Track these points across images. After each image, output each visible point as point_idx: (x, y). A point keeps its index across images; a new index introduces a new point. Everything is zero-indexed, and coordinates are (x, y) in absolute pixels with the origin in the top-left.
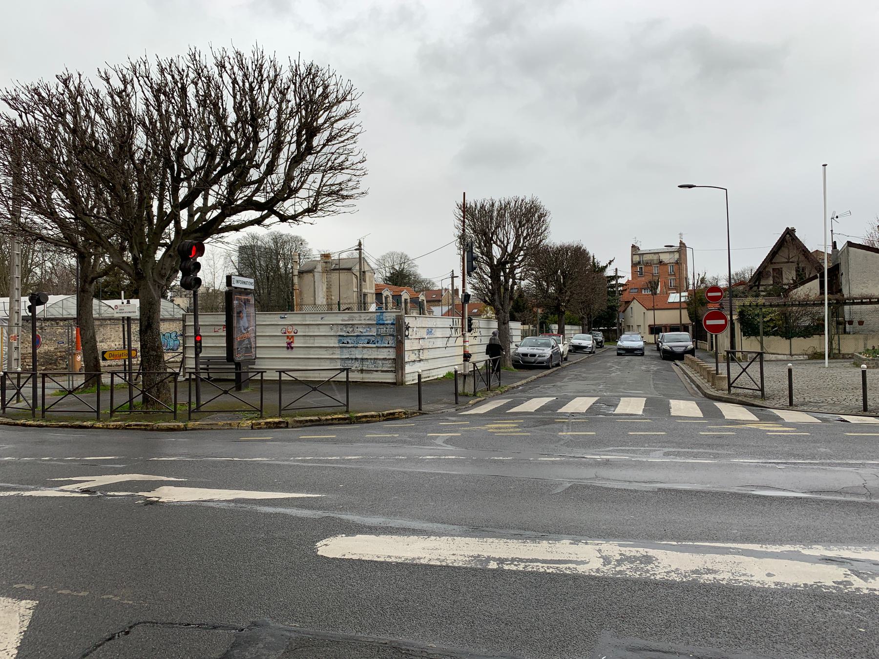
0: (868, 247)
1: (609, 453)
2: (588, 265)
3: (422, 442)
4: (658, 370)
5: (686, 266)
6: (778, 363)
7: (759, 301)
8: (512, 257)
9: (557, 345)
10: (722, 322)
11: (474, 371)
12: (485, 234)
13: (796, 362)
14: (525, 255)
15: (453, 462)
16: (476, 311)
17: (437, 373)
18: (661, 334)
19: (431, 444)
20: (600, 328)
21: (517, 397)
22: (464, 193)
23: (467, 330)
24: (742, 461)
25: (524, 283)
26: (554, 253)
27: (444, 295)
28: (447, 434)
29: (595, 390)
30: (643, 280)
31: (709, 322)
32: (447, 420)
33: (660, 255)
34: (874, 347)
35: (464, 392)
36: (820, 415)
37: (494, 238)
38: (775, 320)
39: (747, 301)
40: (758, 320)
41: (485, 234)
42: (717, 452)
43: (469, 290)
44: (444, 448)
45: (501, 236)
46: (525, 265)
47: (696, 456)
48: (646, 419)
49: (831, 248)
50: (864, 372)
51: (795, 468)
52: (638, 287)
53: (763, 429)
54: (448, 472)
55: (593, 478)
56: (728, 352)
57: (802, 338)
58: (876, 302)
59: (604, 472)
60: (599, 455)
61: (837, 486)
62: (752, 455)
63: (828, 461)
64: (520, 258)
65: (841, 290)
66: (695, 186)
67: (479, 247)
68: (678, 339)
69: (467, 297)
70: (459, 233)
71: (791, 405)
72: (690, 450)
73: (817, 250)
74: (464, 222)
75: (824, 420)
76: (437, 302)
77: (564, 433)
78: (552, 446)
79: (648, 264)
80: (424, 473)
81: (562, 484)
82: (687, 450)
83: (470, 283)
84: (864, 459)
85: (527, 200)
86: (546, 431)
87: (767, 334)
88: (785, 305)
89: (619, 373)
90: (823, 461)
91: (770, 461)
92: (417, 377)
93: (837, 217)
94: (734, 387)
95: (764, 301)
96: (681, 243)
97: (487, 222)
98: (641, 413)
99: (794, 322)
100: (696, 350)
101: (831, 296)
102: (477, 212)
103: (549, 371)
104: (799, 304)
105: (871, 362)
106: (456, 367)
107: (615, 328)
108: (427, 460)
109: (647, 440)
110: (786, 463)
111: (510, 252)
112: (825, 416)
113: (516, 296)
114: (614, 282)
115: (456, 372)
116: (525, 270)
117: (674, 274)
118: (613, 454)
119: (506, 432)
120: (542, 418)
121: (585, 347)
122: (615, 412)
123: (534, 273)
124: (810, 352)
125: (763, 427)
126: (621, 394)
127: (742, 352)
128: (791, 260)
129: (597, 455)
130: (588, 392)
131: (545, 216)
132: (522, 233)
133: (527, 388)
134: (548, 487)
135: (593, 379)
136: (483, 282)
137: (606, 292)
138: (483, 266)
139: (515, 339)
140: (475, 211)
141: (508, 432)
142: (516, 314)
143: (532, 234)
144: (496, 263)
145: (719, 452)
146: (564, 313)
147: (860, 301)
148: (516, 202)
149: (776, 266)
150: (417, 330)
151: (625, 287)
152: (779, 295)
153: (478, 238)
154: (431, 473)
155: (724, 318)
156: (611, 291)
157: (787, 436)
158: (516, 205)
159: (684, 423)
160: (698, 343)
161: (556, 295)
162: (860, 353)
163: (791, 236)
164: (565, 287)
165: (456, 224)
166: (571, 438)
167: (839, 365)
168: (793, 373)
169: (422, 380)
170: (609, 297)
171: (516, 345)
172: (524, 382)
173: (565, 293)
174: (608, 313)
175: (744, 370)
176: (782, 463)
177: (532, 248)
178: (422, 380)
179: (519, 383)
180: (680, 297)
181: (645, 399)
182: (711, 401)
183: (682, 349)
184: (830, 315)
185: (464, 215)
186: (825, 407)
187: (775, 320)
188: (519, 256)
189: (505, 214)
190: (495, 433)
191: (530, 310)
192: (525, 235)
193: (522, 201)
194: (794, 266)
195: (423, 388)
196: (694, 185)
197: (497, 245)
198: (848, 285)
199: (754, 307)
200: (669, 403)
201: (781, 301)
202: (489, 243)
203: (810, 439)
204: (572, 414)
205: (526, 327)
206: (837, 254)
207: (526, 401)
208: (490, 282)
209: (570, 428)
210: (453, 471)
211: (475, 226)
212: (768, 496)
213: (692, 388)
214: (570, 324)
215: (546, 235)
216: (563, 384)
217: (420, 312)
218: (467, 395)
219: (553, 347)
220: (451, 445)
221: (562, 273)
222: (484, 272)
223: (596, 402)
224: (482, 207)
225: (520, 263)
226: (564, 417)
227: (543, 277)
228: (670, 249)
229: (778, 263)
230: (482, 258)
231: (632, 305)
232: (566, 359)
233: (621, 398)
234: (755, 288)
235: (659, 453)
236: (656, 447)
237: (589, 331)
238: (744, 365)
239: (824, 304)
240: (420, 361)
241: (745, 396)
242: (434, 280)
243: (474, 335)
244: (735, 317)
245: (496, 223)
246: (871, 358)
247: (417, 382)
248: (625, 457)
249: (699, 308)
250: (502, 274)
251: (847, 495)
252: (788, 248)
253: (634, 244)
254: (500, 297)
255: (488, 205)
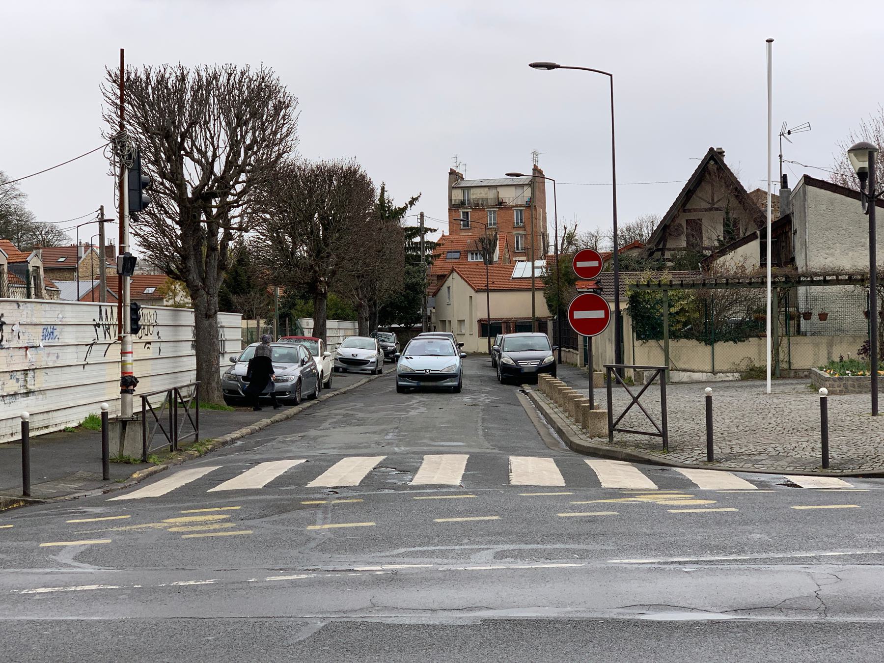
0: (836, 185)
1: (398, 560)
2: (370, 205)
3: (27, 560)
4: (491, 402)
5: (545, 213)
6: (695, 386)
7: (662, 277)
8: (224, 184)
9: (310, 358)
10: (600, 314)
11: (144, 411)
12: (167, 136)
13: (721, 385)
14: (249, 182)
15: (94, 596)
16: (151, 290)
17: (64, 419)
18: (499, 336)
19: (47, 564)
20: (393, 326)
21: (230, 462)
22: (122, 51)
23: (129, 329)
24: (626, 561)
25: (249, 236)
26: (306, 180)
27: (84, 256)
28: (82, 542)
29: (378, 443)
30: (469, 236)
31: (579, 315)
32: (84, 514)
33: (499, 189)
34: (842, 358)
35: (121, 456)
36: (755, 477)
37: (187, 144)
38: (688, 312)
39: (645, 276)
40: (662, 311)
41: (167, 136)
42: (585, 547)
43: (134, 248)
44: (75, 570)
45: (200, 142)
46: (249, 201)
47: (549, 556)
48: (466, 493)
49: (779, 187)
50: (823, 401)
51: (712, 570)
52: (460, 248)
53: (664, 503)
54: (81, 618)
55: (367, 608)
56: (609, 369)
57: (731, 343)
58: (846, 280)
59: (387, 596)
60: (381, 564)
61: (777, 597)
62: (644, 550)
63: (764, 555)
64: (239, 188)
65: (793, 260)
66: (558, 67)
67: (156, 162)
68: (528, 345)
69: (129, 262)
70: (110, 130)
71: (711, 460)
72: (540, 546)
73: (758, 189)
74: (122, 109)
75: (761, 485)
76: (69, 271)
77: (317, 527)
78: (294, 553)
79: (478, 206)
80: (29, 622)
81: (307, 624)
82: (534, 546)
83: (137, 234)
84: (818, 549)
85: (252, 73)
86: (283, 524)
87: (675, 336)
88: (704, 285)
89: (423, 409)
90: (756, 555)
91: (671, 560)
92: (20, 428)
93: (789, 133)
94: (620, 431)
95: (670, 277)
96: (536, 169)
97: (172, 112)
98: (458, 482)
99: (718, 314)
100: (558, 366)
101: (778, 270)
102: (150, 91)
103: (292, 410)
104: (727, 284)
105: (836, 384)
106: (105, 405)
107: (419, 325)
108: (37, 597)
109: (467, 532)
110: (697, 562)
111: (219, 175)
112: (764, 478)
113: (231, 263)
114: (417, 239)
115: (104, 414)
116: (249, 210)
117: (524, 227)
118: (406, 560)
119: (205, 532)
120: (276, 500)
121: (364, 362)
122: (412, 483)
123: (268, 216)
124: (743, 366)
125: (662, 499)
126: (425, 448)
127: (634, 368)
128: (716, 206)
129: (377, 563)
130: (365, 447)
131: (288, 106)
132: (244, 137)
133: (252, 441)
134: (282, 632)
135: (377, 422)
136: (163, 233)
137: (403, 257)
138: (164, 199)
139: (229, 347)
140: (147, 88)
141: (209, 531)
142: (234, 298)
143: (263, 140)
144: (190, 195)
145: (590, 547)
146: (324, 295)
147: (821, 278)
148: (230, 75)
149: (692, 216)
150: (22, 329)
151: (439, 250)
152: (695, 268)
153: (154, 143)
154: (45, 622)
155: (603, 306)
156: (412, 256)
157: (701, 514)
158: (231, 82)
159: (532, 497)
160: (563, 353)
161: (309, 262)
162: (821, 369)
163: (716, 162)
164: (327, 246)
165: (106, 112)
166: (330, 535)
167: (788, 389)
168: (714, 405)
169: (31, 434)
170: (408, 266)
171: (232, 360)
172: (245, 431)
173: (328, 257)
174: (406, 297)
175: (635, 400)
176: (691, 562)
177: (262, 169)
178: (31, 434)
179: (235, 435)
180: (533, 268)
181: (467, 456)
182: (577, 457)
183: (535, 364)
184: (776, 302)
185: (122, 94)
186: (764, 462)
187: (688, 312)
188: (237, 182)
189: (207, 100)
190: (183, 533)
191: (261, 290)
192: (248, 142)
193: (243, 73)
194: (720, 216)
195: (32, 450)
196: (557, 63)
197: (193, 159)
198: (804, 251)
199: (655, 288)
200: (508, 463)
201: (699, 278)
202: (175, 154)
203: (737, 518)
204: (335, 490)
205: (253, 323)
206: (788, 197)
207: (248, 468)
208: (179, 232)
209: (330, 515)
210: (92, 614)
211: (146, 119)
212: (666, 623)
213: (550, 434)
214: (337, 317)
215: (289, 144)
216: (319, 433)
217: (29, 289)
218: (127, 462)
219: (303, 362)
220: (90, 563)
221: (321, 218)
222: (166, 212)
223: (380, 465)
224: (162, 80)
225: (240, 197)
226: (319, 496)
227: (284, 227)
228: (517, 181)
229: (695, 210)
230: (162, 184)
231: (449, 282)
232: (327, 385)
233: (425, 457)
234: (658, 255)
235: (488, 555)
236: (482, 543)
237: (371, 330)
238: (635, 390)
239: (766, 282)
240: (28, 394)
241: (637, 446)
242: (61, 227)
243: (145, 339)
244: (623, 306)
245: (190, 115)
246: (837, 376)
247: (20, 438)
248: (426, 565)
249: (564, 289)
250: (203, 217)
251: (790, 611)
252: (713, 185)
253: (454, 168)
254: (199, 263)
255: (173, 78)
